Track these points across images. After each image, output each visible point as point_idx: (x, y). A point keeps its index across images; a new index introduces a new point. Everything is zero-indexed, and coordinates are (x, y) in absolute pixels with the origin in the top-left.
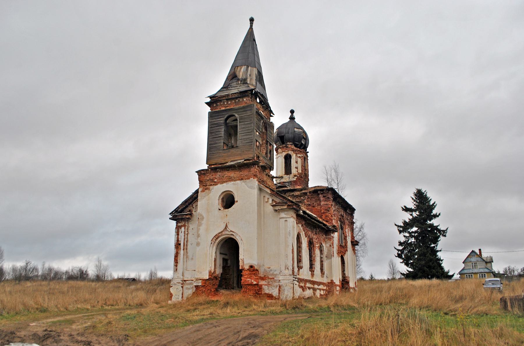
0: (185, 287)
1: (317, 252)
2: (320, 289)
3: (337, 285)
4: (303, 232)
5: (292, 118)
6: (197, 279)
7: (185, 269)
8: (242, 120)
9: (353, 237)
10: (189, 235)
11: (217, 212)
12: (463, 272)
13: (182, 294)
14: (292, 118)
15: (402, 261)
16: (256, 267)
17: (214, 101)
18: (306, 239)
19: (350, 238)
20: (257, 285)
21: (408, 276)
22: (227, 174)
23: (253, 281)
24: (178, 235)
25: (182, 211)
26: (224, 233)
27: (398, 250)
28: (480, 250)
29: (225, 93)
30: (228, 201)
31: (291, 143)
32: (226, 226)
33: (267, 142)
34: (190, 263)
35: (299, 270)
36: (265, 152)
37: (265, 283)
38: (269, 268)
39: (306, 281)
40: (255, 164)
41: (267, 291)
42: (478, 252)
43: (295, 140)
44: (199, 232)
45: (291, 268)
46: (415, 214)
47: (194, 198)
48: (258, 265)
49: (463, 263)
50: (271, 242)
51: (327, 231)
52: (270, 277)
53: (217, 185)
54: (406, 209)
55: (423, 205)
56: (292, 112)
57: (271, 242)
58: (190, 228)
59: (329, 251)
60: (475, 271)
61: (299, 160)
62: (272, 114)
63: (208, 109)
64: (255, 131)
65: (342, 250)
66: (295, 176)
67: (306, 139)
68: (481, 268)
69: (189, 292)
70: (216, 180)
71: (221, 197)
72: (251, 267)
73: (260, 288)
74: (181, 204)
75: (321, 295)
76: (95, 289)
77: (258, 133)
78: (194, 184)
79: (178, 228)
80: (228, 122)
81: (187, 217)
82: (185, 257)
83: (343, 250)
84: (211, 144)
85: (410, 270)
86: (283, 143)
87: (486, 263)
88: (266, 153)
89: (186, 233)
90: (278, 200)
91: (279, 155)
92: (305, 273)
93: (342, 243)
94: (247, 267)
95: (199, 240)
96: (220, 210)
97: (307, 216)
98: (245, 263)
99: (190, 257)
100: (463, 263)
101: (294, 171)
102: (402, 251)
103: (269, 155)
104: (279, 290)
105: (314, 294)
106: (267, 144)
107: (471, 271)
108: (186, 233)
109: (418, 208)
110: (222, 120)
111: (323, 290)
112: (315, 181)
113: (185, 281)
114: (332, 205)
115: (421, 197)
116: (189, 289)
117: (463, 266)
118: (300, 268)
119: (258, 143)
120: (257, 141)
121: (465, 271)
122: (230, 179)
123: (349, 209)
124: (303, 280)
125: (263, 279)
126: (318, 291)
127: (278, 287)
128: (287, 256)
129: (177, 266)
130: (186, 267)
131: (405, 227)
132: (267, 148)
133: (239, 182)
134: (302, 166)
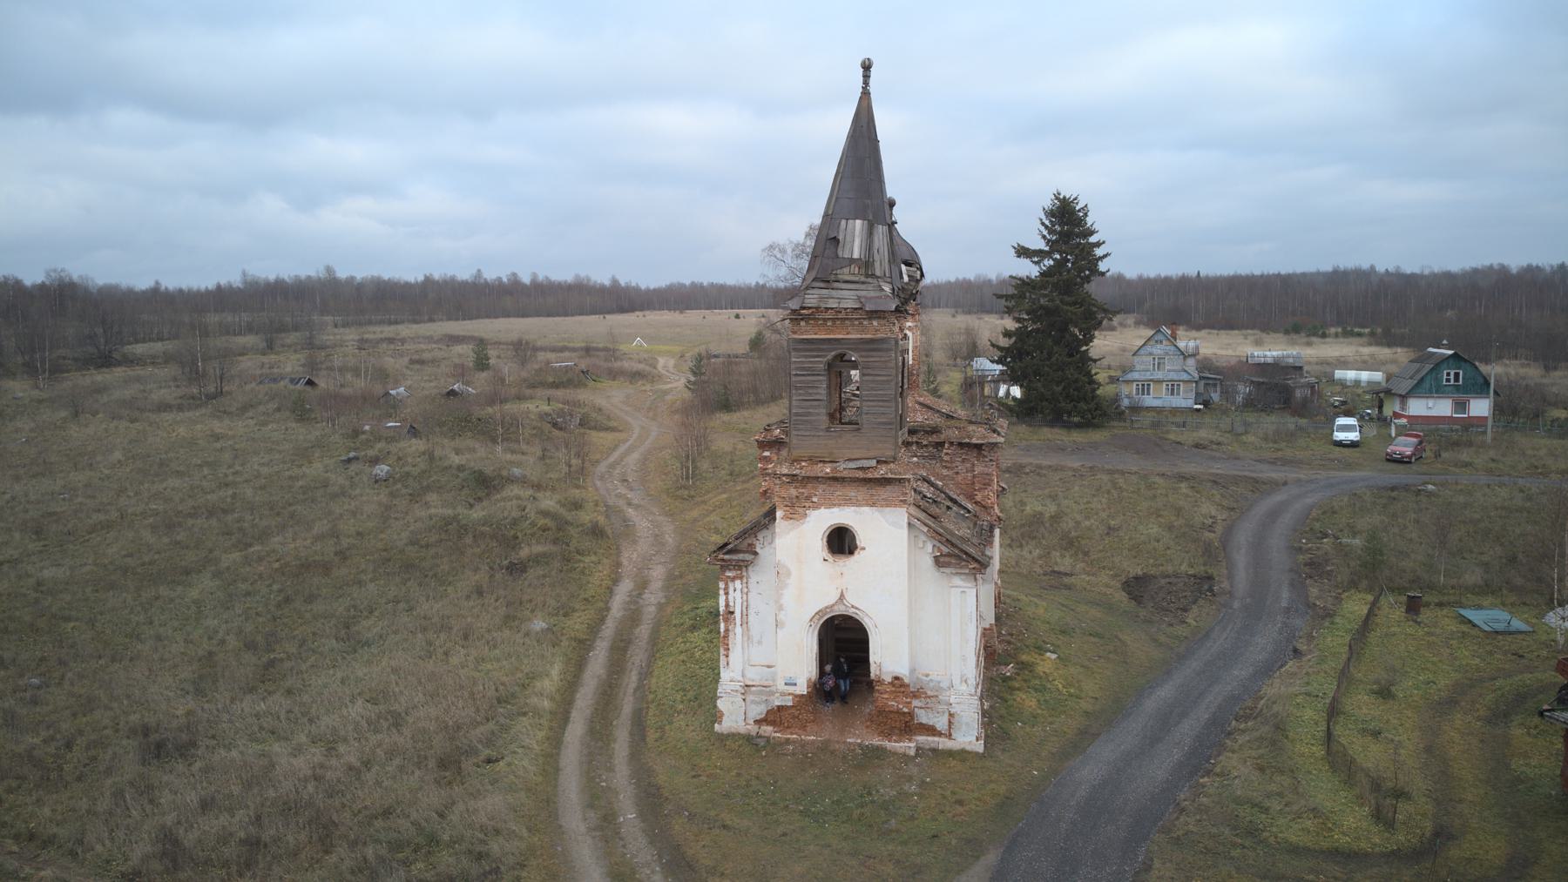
6: (783, 694)
11: (819, 563)
16: (906, 681)
27: (999, 348)
30: (841, 542)
41: (924, 720)
54: (1022, 252)
60: (1159, 375)
72: (897, 678)
76: (76, 414)
90: (945, 550)
107: (1148, 376)
122: (848, 502)
125: (915, 695)
133: (866, 509)
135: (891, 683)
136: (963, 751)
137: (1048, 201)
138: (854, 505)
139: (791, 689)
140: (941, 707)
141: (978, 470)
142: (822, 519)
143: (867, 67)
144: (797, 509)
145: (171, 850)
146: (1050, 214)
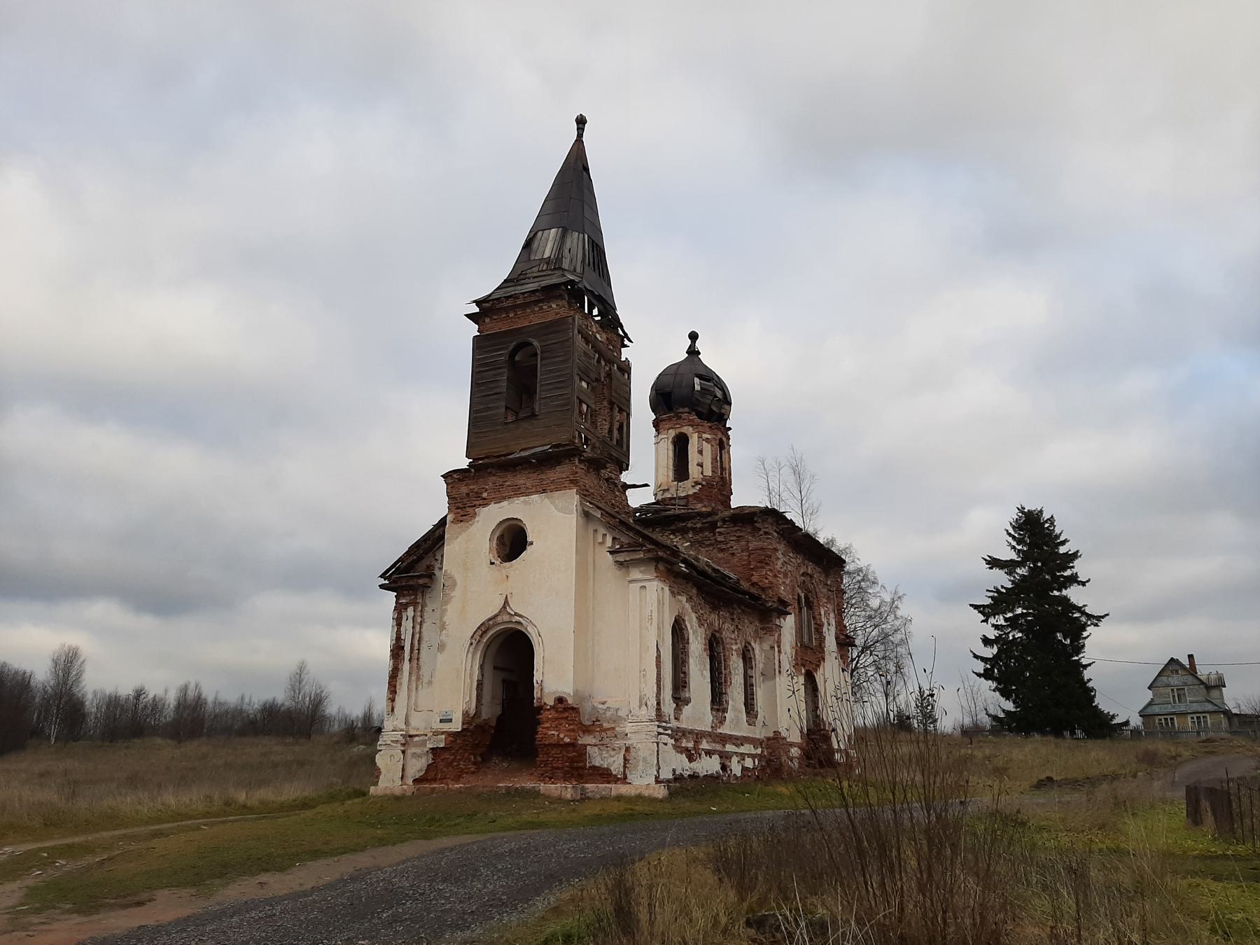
0: (409, 752)
1: (736, 664)
2: (742, 756)
3: (792, 745)
4: (694, 616)
5: (693, 352)
6: (436, 733)
7: (413, 708)
8: (547, 354)
9: (841, 627)
10: (424, 626)
11: (485, 568)
12: (1149, 711)
13: (403, 770)
14: (693, 352)
15: (994, 685)
17: (486, 310)
18: (701, 631)
19: (833, 629)
20: (573, 745)
21: (1004, 724)
22: (510, 480)
23: (562, 736)
24: (399, 625)
25: (410, 567)
26: (499, 619)
27: (984, 660)
28: (1191, 657)
29: (512, 291)
30: (513, 542)
31: (687, 409)
32: (506, 602)
33: (611, 404)
34: (423, 692)
35: (678, 709)
36: (607, 427)
37: (594, 741)
38: (603, 703)
39: (699, 736)
40: (574, 456)
41: (597, 762)
42: (1186, 662)
43: (694, 399)
44: (445, 619)
45: (653, 702)
46: (1021, 571)
47: (433, 541)
48: (576, 692)
49: (1150, 688)
50: (606, 638)
51: (764, 612)
52: (606, 725)
53: (487, 504)
54: (994, 563)
55: (1039, 550)
56: (693, 337)
57: (606, 638)
58: (428, 609)
59: (769, 660)
61: (707, 448)
62: (626, 342)
63: (473, 329)
64: (577, 378)
65: (808, 659)
66: (697, 483)
67: (727, 401)
68: (1193, 701)
69: (417, 766)
70: (485, 495)
71: (498, 534)
72: (560, 700)
73: (581, 752)
74: (408, 553)
75: (744, 769)
77: (584, 384)
78: (436, 506)
79: (400, 609)
80: (517, 358)
81: (421, 581)
82: (414, 678)
83: (810, 657)
84: (477, 412)
85: (1009, 706)
86: (670, 409)
87: (1208, 688)
88: (610, 431)
89: (419, 620)
91: (661, 436)
92: (698, 713)
93: (810, 639)
94: (550, 702)
95: (443, 637)
96: (492, 563)
97: (695, 574)
98: (546, 690)
99: (425, 680)
100: (1150, 688)
101: (694, 470)
102: (993, 661)
103: (616, 433)
104: (625, 759)
105: (724, 767)
106: (611, 409)
107: (1170, 709)
108: (419, 620)
109: (1026, 557)
110: (502, 355)
111: (753, 756)
112: (744, 495)
113: (411, 736)
114: (776, 550)
115: (1034, 531)
116: (420, 756)
117: (1149, 695)
118: (680, 700)
119: (585, 407)
120: (581, 402)
121: (1156, 709)
122: (518, 492)
123: (827, 561)
124: (691, 732)
125: (587, 730)
126: (735, 759)
127: (623, 752)
128: (643, 673)
129: (393, 700)
130: (416, 704)
131: (999, 603)
132: (612, 417)
133: (535, 497)
134: (714, 460)
136: (639, 797)
137: (1014, 515)
140: (619, 743)
141: (751, 546)
143: (581, 122)
146: (1018, 526)
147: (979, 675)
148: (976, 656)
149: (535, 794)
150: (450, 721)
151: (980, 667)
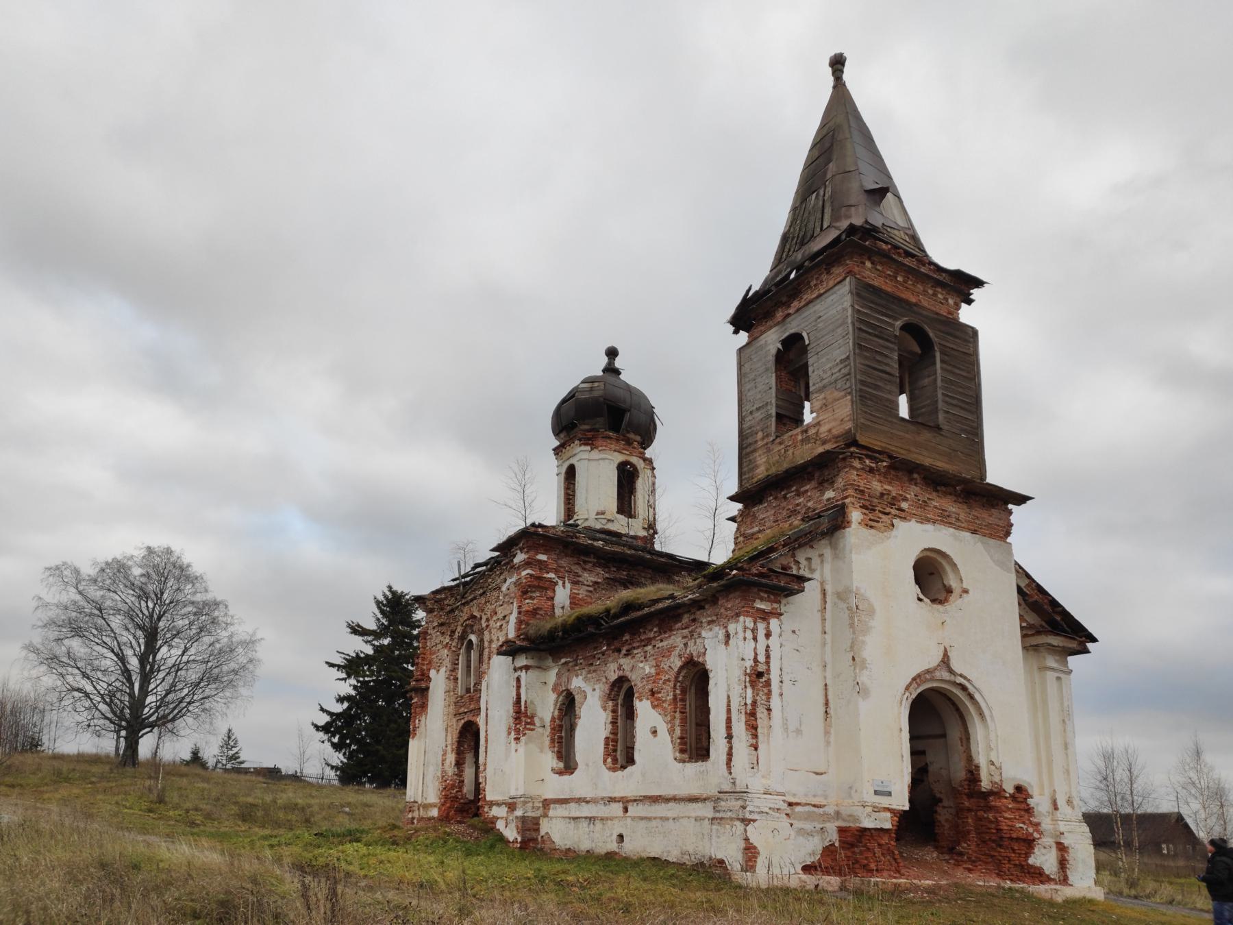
5: (611, 370)
6: (877, 809)
14: (611, 370)
54: (357, 630)
70: (904, 505)
96: (920, 600)
133: (967, 535)
135: (1013, 797)
137: (380, 592)
138: (950, 524)
139: (884, 802)
142: (913, 537)
143: (838, 63)
144: (881, 512)
145: (953, 808)
147: (317, 728)
148: (322, 710)
149: (1028, 896)
150: (889, 794)
151: (324, 719)
